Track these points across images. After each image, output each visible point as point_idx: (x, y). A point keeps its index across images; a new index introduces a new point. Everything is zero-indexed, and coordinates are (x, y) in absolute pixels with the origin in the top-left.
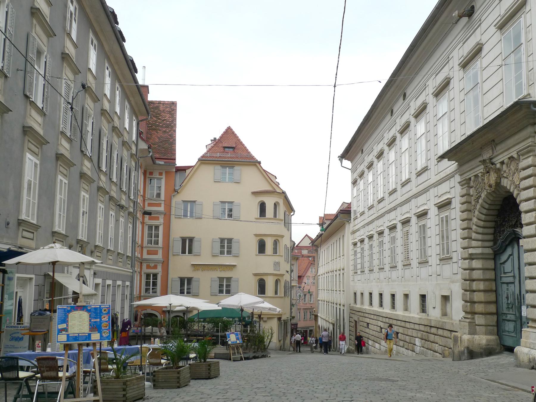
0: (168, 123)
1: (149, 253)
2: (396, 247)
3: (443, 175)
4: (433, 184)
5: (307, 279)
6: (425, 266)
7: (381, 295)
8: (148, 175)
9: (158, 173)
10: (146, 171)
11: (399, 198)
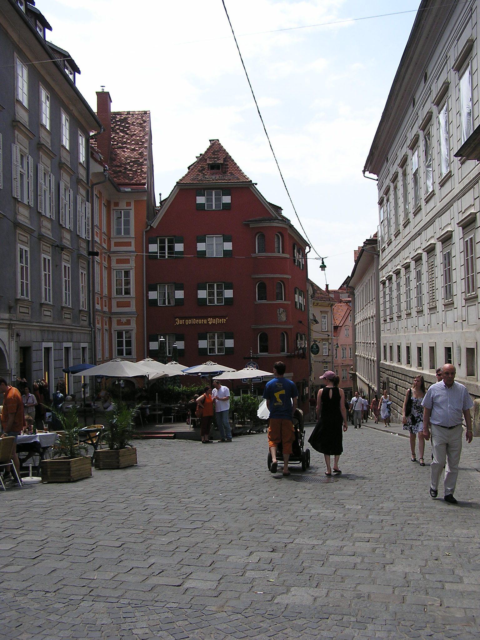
0: (138, 138)
1: (119, 305)
2: (421, 284)
3: (466, 181)
4: (456, 195)
5: (346, 330)
6: (451, 309)
7: (408, 348)
8: (112, 207)
9: (125, 203)
10: (110, 201)
11: (424, 218)
